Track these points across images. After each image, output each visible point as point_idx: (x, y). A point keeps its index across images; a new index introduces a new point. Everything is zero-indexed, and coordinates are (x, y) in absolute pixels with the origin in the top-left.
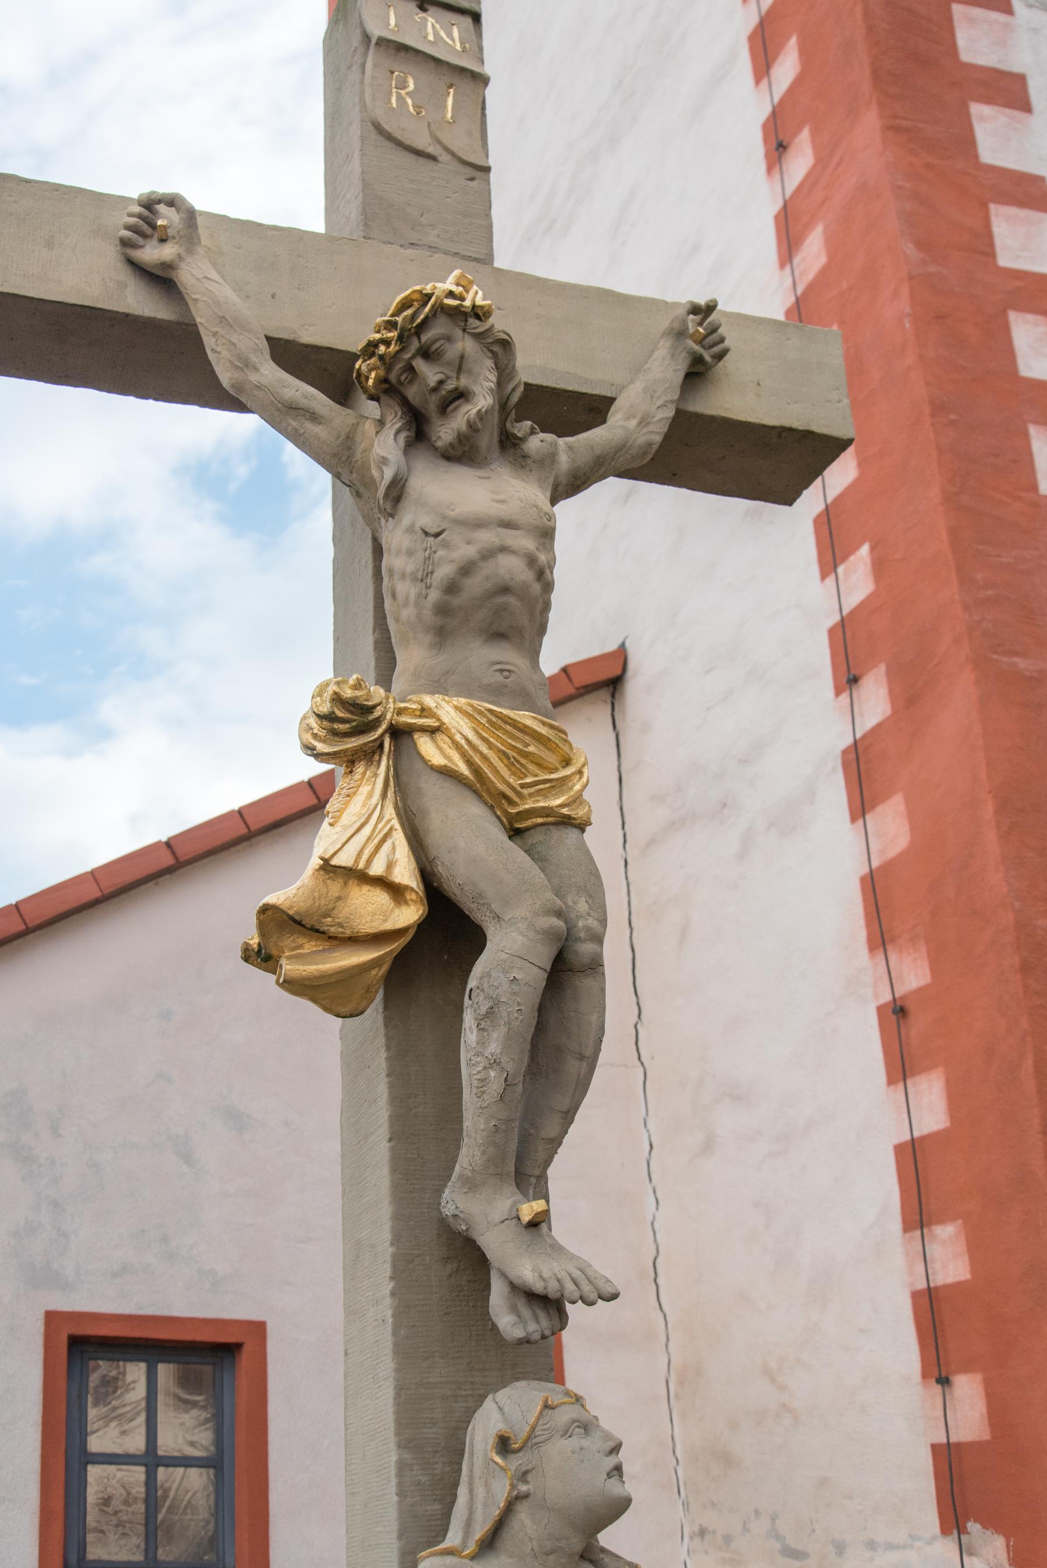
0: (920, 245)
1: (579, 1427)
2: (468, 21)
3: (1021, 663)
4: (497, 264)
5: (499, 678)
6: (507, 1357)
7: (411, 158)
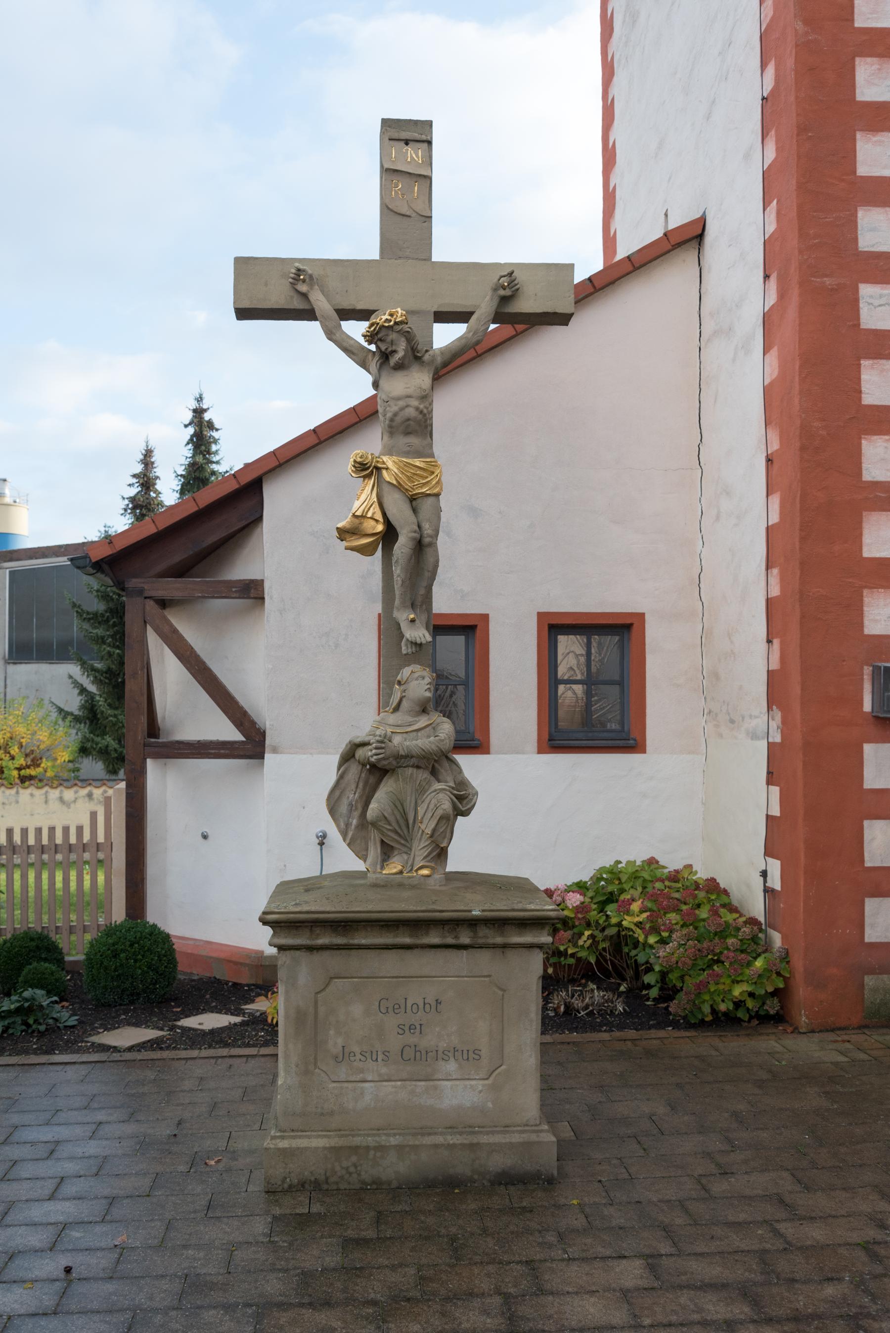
0: (806, 22)
2: (426, 145)
3: (828, 281)
4: (433, 260)
5: (408, 449)
7: (399, 218)
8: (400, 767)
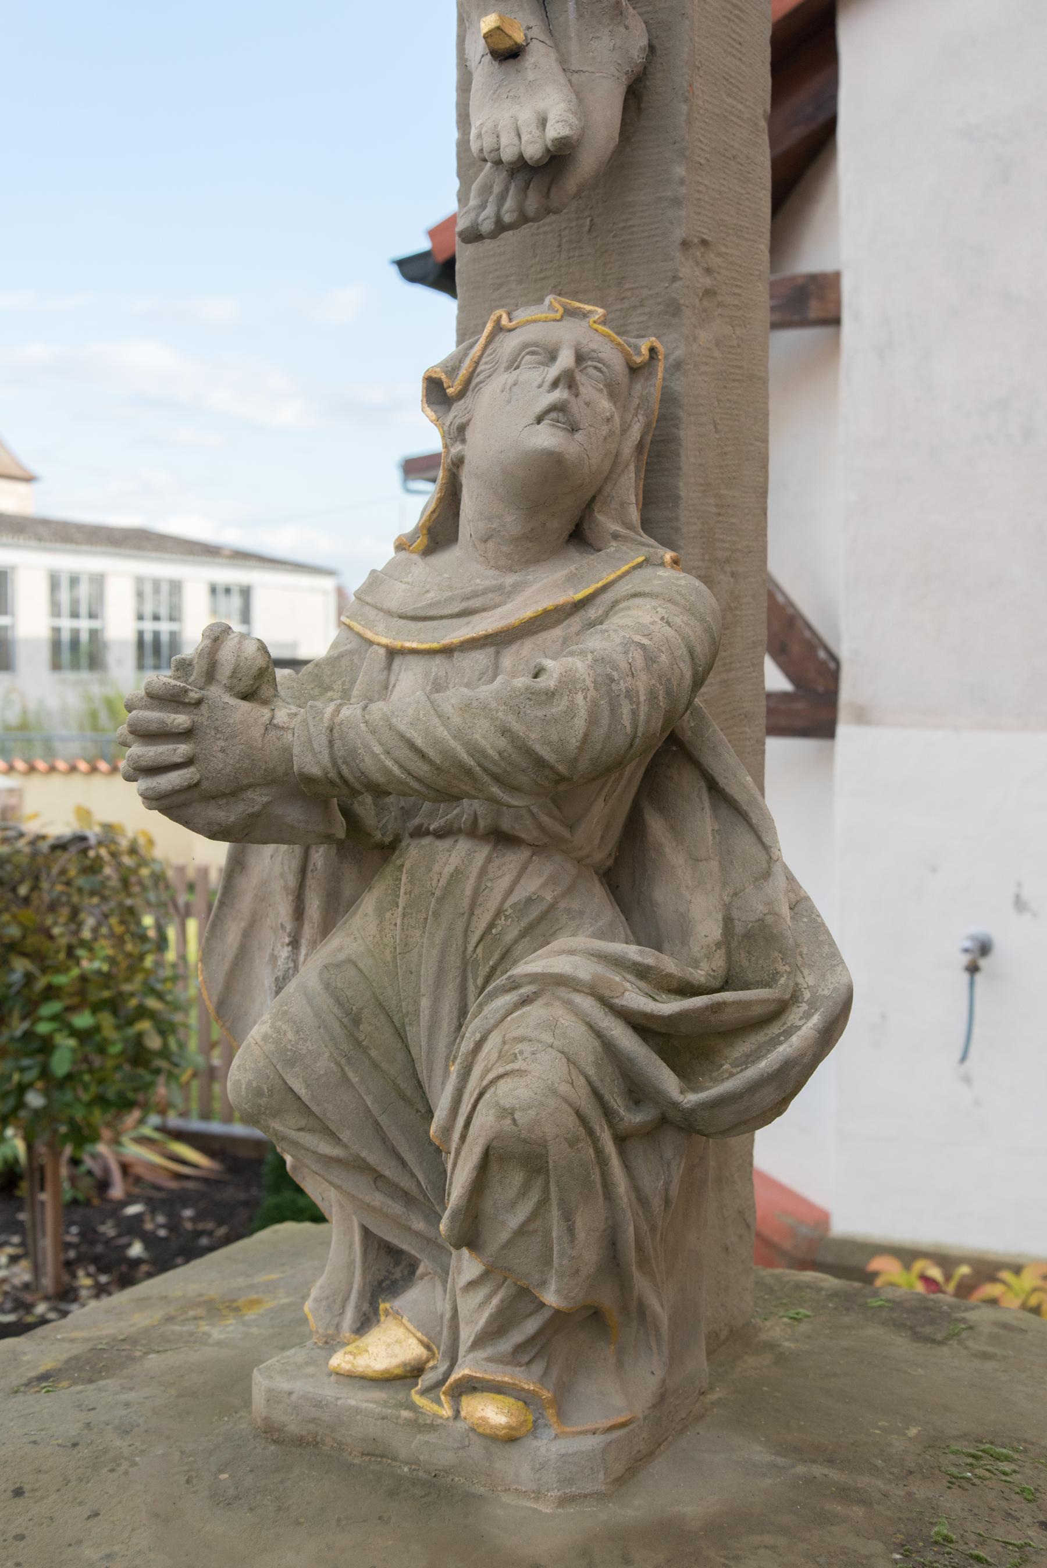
1: (533, 353)
6: (610, 268)
8: (419, 833)
